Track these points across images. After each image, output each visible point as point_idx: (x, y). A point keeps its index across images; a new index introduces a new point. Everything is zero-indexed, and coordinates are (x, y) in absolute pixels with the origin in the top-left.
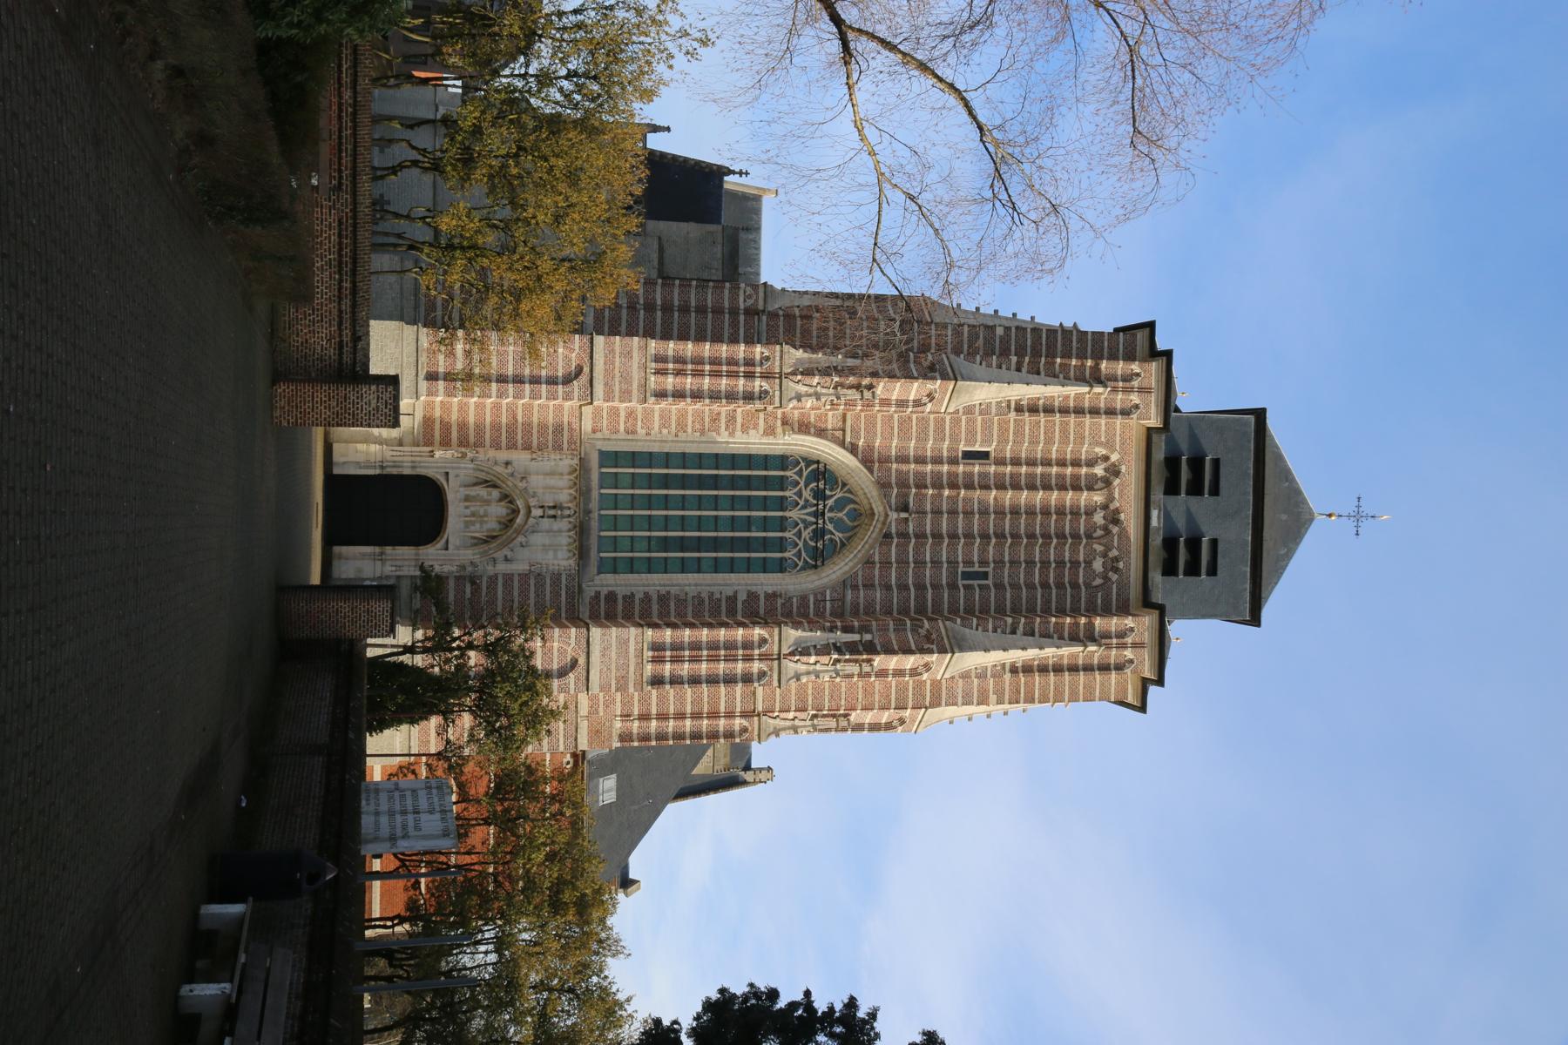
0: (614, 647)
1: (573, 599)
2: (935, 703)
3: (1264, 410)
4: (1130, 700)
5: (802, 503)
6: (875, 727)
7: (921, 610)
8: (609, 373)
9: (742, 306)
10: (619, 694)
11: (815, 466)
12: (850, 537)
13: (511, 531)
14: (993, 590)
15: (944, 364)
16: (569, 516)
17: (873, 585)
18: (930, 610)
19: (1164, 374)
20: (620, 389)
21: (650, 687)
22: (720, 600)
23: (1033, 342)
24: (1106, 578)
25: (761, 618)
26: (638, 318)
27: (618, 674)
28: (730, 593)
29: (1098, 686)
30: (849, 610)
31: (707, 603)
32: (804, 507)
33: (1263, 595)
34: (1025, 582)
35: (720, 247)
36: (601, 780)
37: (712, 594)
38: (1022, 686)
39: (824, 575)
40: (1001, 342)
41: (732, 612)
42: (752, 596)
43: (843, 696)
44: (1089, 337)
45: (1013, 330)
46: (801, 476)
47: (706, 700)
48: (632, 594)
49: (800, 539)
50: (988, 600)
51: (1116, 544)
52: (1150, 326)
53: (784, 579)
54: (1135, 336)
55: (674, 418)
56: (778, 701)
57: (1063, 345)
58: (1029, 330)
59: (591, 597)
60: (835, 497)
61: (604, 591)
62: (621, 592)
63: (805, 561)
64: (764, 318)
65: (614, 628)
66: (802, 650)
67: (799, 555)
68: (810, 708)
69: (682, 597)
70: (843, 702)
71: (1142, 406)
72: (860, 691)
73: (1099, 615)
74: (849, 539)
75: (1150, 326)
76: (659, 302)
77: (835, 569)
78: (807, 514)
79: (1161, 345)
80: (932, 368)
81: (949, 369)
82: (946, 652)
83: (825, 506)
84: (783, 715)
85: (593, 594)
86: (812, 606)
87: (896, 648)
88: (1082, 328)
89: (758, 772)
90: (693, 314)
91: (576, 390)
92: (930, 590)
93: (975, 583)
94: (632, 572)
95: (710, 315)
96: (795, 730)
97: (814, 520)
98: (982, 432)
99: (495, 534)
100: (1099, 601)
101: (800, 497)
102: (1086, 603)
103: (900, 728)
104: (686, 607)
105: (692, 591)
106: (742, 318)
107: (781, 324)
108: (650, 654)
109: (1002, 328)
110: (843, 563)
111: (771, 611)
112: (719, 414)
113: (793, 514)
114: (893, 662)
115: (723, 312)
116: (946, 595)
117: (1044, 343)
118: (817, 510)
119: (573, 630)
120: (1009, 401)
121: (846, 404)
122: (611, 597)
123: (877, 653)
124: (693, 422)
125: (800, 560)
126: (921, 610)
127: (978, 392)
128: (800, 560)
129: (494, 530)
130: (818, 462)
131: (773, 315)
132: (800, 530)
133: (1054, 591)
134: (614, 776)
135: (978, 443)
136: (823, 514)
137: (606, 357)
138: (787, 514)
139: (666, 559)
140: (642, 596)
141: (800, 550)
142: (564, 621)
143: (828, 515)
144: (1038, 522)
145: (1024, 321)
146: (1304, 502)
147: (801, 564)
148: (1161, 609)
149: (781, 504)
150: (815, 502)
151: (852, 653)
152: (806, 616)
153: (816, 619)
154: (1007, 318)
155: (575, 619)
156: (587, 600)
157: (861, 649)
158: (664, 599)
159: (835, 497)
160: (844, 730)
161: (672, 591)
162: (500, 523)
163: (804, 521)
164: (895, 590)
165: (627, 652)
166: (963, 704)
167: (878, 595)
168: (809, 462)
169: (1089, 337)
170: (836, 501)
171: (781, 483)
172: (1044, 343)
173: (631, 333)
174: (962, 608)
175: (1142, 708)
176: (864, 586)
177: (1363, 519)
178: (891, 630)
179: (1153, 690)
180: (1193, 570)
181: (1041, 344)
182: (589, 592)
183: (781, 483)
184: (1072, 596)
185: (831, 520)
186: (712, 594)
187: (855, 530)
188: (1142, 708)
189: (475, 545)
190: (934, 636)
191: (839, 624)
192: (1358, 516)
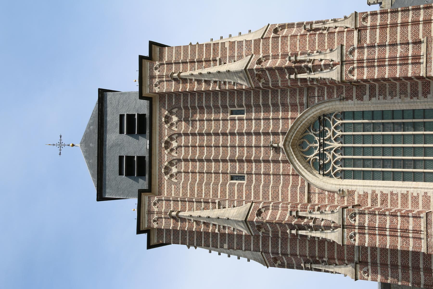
2: (257, 42)
3: (98, 200)
4: (158, 49)
5: (332, 152)
6: (291, 26)
7: (265, 93)
9: (369, 267)
11: (325, 173)
12: (305, 133)
14: (228, 105)
15: (253, 230)
18: (261, 93)
19: (141, 221)
21: (422, 40)
22: (380, 95)
23: (209, 239)
25: (354, 85)
28: (373, 99)
29: (174, 55)
30: (305, 91)
32: (331, 149)
33: (98, 105)
34: (212, 110)
37: (384, 98)
38: (212, 53)
39: (319, 111)
40: (225, 240)
41: (372, 88)
42: (360, 98)
43: (307, 42)
46: (333, 167)
50: (230, 99)
51: (166, 130)
52: (149, 246)
53: (342, 108)
54: (158, 241)
55: (410, 202)
56: (345, 38)
57: (193, 237)
58: (211, 246)
63: (330, 119)
64: (356, 259)
67: (334, 122)
68: (326, 35)
69: (403, 96)
70: (308, 39)
71: (152, 204)
72: (298, 46)
73: (173, 92)
74: (306, 132)
75: (149, 246)
76: (422, 273)
77: (312, 115)
78: (330, 145)
79: (144, 236)
80: (259, 228)
81: (250, 227)
82: (249, 70)
83: (319, 150)
86: (326, 93)
87: (276, 71)
88: (185, 246)
90: (399, 264)
92: (261, 103)
93: (237, 109)
95: (389, 263)
97: (326, 142)
98: (234, 191)
100: (174, 100)
101: (333, 155)
102: (180, 99)
103: (277, 26)
104: (400, 90)
105: (397, 99)
106: (369, 260)
107: (346, 256)
108: (421, 61)
109: (225, 248)
110: (308, 118)
111: (349, 90)
112: (382, 204)
113: (336, 145)
114: (278, 63)
115: (381, 264)
116: (252, 101)
117: (203, 239)
118: (323, 148)
120: (219, 208)
121: (307, 208)
124: (397, 199)
125: (333, 119)
126: (265, 93)
127: (235, 214)
128: (333, 119)
130: (324, 175)
131: (351, 261)
132: (333, 136)
133: (196, 105)
135: (236, 184)
136: (320, 145)
138: (341, 145)
139: (414, 118)
141: (333, 125)
143: (318, 145)
144: (205, 142)
147: (333, 117)
148: (141, 96)
149: (343, 150)
150: (325, 152)
152: (328, 87)
154: (224, 252)
157: (296, 70)
158: (414, 94)
161: (409, 99)
163: (331, 141)
166: (242, 41)
168: (329, 175)
170: (313, 153)
172: (203, 239)
174: (244, 95)
175: (151, 44)
176: (297, 105)
177: (58, 143)
178: (280, 81)
179: (147, 54)
180: (131, 117)
181: (204, 238)
184: (188, 103)
185: (316, 143)
186: (384, 98)
187: (302, 136)
188: (151, 44)
190: (256, 78)
191: (309, 83)
192: (61, 145)
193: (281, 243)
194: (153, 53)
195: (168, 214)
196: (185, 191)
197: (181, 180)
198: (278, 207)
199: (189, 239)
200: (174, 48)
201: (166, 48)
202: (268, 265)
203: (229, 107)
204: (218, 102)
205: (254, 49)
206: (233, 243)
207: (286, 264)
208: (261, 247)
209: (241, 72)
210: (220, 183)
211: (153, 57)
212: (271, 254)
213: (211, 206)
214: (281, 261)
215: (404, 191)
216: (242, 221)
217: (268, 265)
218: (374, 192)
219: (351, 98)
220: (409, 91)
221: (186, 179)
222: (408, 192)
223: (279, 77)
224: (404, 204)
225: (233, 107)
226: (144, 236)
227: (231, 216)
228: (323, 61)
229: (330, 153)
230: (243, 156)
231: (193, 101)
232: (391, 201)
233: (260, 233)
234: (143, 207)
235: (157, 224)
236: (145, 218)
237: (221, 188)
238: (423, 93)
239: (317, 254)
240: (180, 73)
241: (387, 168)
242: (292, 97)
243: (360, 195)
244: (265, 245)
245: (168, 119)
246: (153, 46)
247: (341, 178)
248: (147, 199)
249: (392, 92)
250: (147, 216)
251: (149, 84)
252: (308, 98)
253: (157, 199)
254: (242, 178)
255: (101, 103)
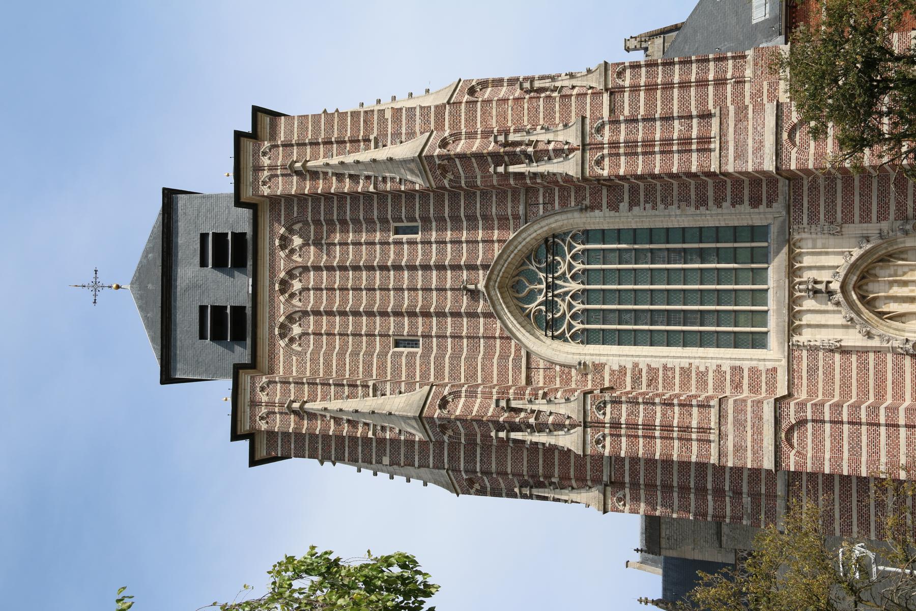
0: (750, 151)
1: (795, 199)
2: (440, 109)
3: (162, 382)
4: (267, 119)
5: (568, 298)
6: (498, 82)
7: (454, 197)
8: (758, 431)
9: (627, 490)
10: (746, 104)
11: (556, 334)
13: (862, 267)
15: (433, 432)
16: (800, 283)
17: (499, 219)
18: (446, 197)
19: (239, 419)
20: (746, 414)
21: (713, 112)
22: (646, 202)
23: (356, 449)
24: (290, 230)
26: (731, 482)
27: (746, 123)
28: (636, 209)
29: (296, 130)
31: (659, 199)
32: (566, 293)
33: (161, 217)
34: (361, 225)
35: (663, 535)
36: (767, 16)
37: (653, 208)
38: (362, 128)
39: (546, 228)
40: (385, 450)
41: (634, 191)
42: (614, 206)
43: (526, 112)
44: (307, 452)
45: (374, 462)
46: (569, 323)
47: (659, 103)
48: (734, 206)
49: (570, 263)
51: (282, 261)
52: (253, 462)
53: (584, 223)
54: (268, 453)
55: (693, 382)
56: (588, 105)
57: (330, 446)
58: (360, 460)
59: (776, 201)
60: (536, 303)
61: (762, 208)
62: (745, 208)
65: (750, 170)
66: (562, 152)
67: (571, 248)
68: (557, 99)
69: (683, 204)
70: (526, 106)
71: (258, 389)
72: (510, 118)
74: (523, 264)
75: (253, 462)
76: (710, 498)
77: (534, 235)
78: (563, 287)
79: (245, 444)
81: (427, 427)
84: (584, 90)
85: (774, 205)
86: (557, 198)
87: (473, 160)
88: (316, 462)
89: (638, 46)
90: (675, 484)
91: (792, 413)
92: (446, 215)
93: (405, 224)
94: (735, 227)
95: (658, 483)
96: (572, 76)
97: (557, 282)
98: (400, 365)
99: (881, 264)
100: (295, 209)
102: (307, 207)
103: (474, 83)
104: (679, 194)
105: (673, 209)
106: (627, 479)
107: (589, 473)
108: (712, 146)
111: (596, 193)
112: (649, 386)
113: (574, 286)
114: (476, 145)
115: (645, 485)
117: (347, 448)
118: (553, 291)
119: (793, 167)
120: (374, 395)
122: (755, 202)
123: (490, 154)
124: (674, 377)
125: (569, 243)
126: (454, 197)
127: (401, 405)
128: (569, 243)
129: (882, 268)
130: (553, 337)
131: (597, 481)
132: (570, 271)
133: (335, 217)
134: (754, 22)
135: (404, 355)
136: (548, 287)
137: (761, 447)
138: (582, 287)
140: (724, 204)
141: (570, 252)
142: (763, 178)
143: (543, 286)
144: (350, 281)
145: (367, 468)
146: (137, 299)
147: (568, 239)
148: (239, 202)
150: (556, 299)
151: (514, 153)
152: (561, 188)
153: (552, 186)
154: (382, 471)
155: (793, 178)
156: (781, 198)
157: (506, 158)
158: (702, 201)
159: (536, 303)
160: (526, 79)
161: (693, 209)
162: (876, 276)
163: (566, 281)
164: (478, 215)
165: (736, 148)
166: (415, 108)
167: (494, 210)
168: (562, 337)
169: (307, 452)
170: (536, 300)
171: (588, 315)
172: (347, 448)
173: (737, 471)
174: (417, 200)
175: (256, 110)
176: (508, 219)
177: (91, 284)
178: (479, 177)
179: (247, 128)
180: (220, 238)
182: (779, 207)
183: (588, 315)
185: (540, 282)
186: (653, 208)
187: (517, 272)
188: (256, 110)
189: (902, 252)
190: (438, 172)
191: (528, 181)
193: (481, 454)
194: (259, 126)
195: (286, 406)
196: (316, 366)
197: (309, 347)
198: (476, 392)
199: (322, 449)
200: (296, 118)
201: (283, 118)
202: (459, 490)
203: (391, 221)
204: (372, 212)
205: (436, 122)
206: (399, 454)
207: (489, 489)
208: (446, 461)
209: (413, 160)
210: (377, 351)
211: (259, 133)
212: (463, 473)
213: (360, 392)
214: (480, 485)
215: (685, 363)
216: (414, 418)
217: (459, 490)
218: (636, 365)
219: (600, 207)
220: (693, 196)
221: (318, 347)
222: (690, 364)
223: (477, 170)
224: (685, 385)
225: (399, 222)
226: (245, 444)
227: (396, 408)
228: (553, 143)
229: (563, 300)
230: (416, 306)
231: (329, 211)
232: (664, 380)
233: (446, 438)
234: (241, 394)
235: (267, 423)
236: (246, 413)
237: (378, 361)
238: (716, 200)
239: (541, 471)
240: (307, 161)
241: (658, 325)
242: (499, 205)
243: (613, 371)
244: (453, 458)
245: (285, 242)
246: (259, 114)
247: (582, 343)
248: (249, 381)
249: (666, 197)
250: (249, 410)
251: (251, 180)
252: (528, 206)
253: (267, 380)
254: (415, 344)
255: (168, 213)
